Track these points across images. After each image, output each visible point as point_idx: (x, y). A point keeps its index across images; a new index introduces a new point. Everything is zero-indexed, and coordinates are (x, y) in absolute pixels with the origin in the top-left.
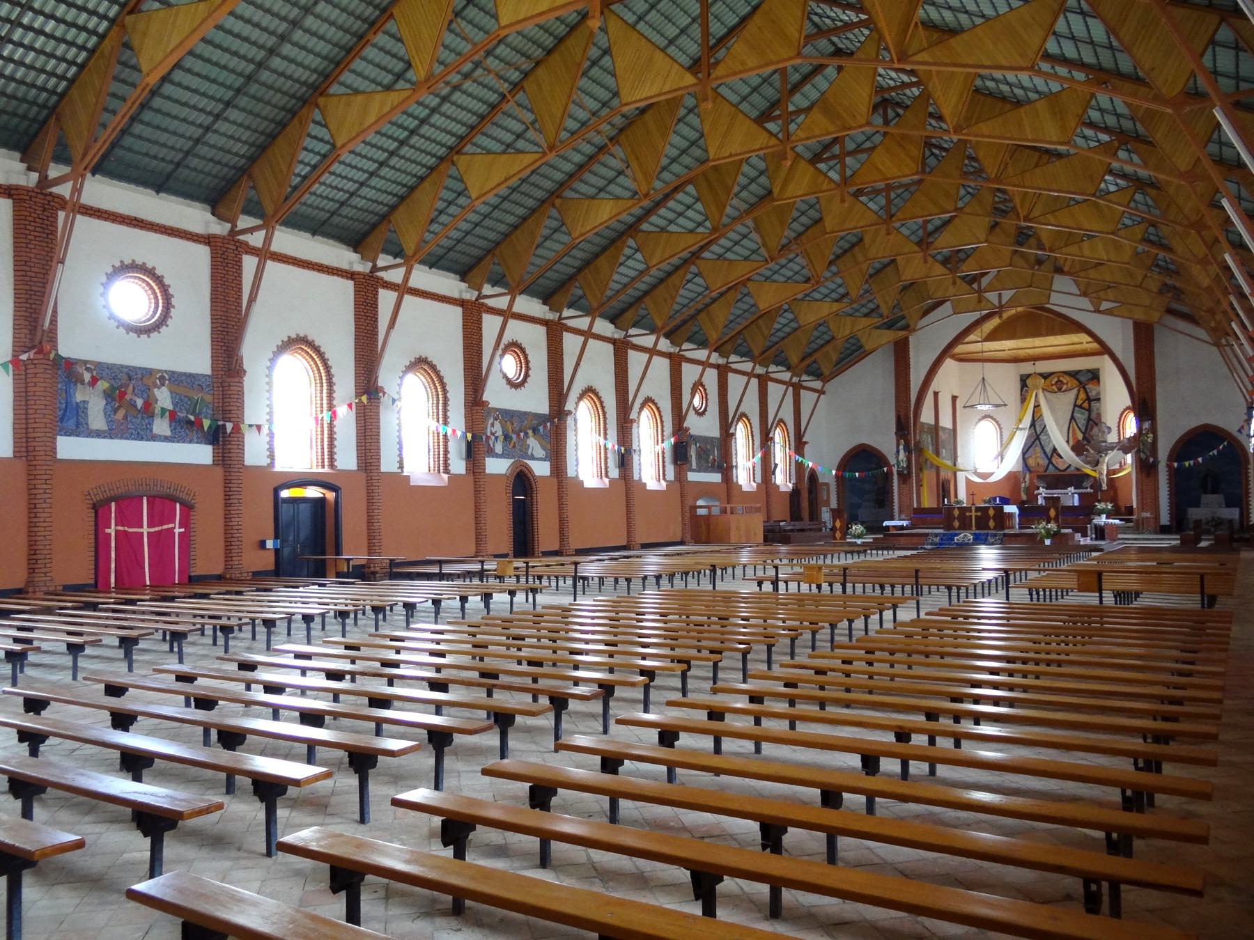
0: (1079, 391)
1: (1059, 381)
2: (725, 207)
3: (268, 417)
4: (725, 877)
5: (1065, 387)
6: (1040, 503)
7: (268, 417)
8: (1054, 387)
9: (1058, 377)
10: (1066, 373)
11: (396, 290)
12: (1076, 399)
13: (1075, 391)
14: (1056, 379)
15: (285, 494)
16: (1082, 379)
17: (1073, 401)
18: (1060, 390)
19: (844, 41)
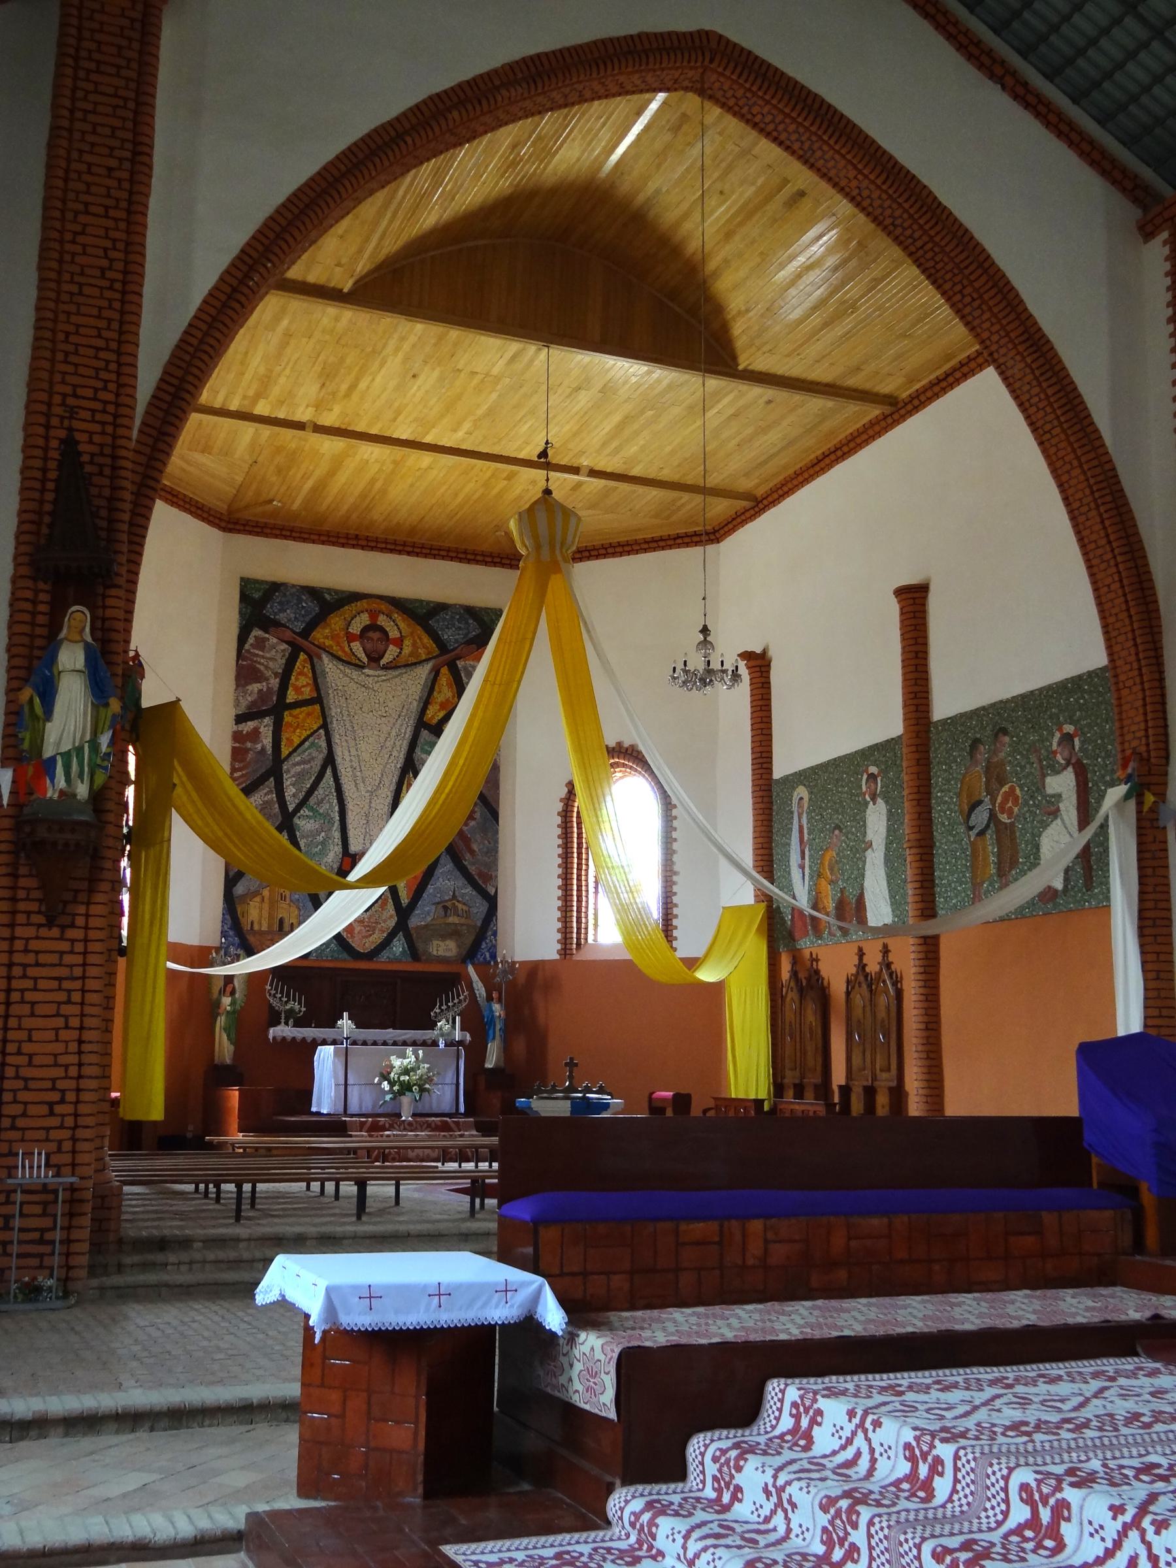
0: (436, 673)
1: (372, 627)
2: (499, 1247)
3: (674, 835)
4: (557, 957)
5: (391, 653)
6: (49, 794)
7: (674, 835)
8: (356, 646)
9: (373, 615)
10: (399, 605)
11: (981, 367)
12: (426, 703)
13: (424, 672)
14: (364, 619)
15: (487, 1181)
16: (447, 635)
17: (415, 706)
18: (374, 658)
19: (227, 1338)
